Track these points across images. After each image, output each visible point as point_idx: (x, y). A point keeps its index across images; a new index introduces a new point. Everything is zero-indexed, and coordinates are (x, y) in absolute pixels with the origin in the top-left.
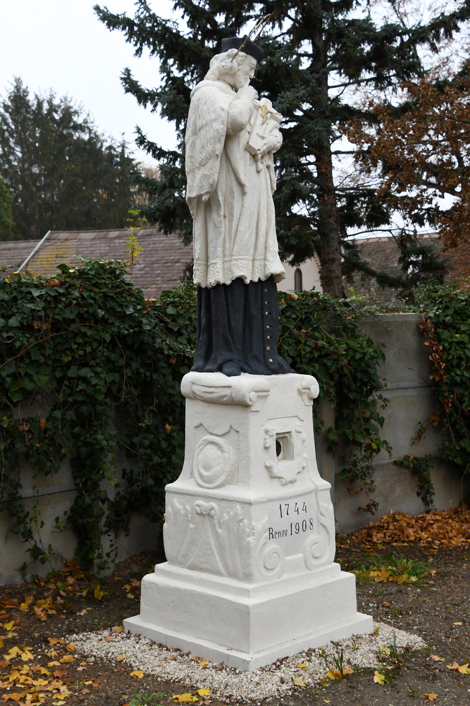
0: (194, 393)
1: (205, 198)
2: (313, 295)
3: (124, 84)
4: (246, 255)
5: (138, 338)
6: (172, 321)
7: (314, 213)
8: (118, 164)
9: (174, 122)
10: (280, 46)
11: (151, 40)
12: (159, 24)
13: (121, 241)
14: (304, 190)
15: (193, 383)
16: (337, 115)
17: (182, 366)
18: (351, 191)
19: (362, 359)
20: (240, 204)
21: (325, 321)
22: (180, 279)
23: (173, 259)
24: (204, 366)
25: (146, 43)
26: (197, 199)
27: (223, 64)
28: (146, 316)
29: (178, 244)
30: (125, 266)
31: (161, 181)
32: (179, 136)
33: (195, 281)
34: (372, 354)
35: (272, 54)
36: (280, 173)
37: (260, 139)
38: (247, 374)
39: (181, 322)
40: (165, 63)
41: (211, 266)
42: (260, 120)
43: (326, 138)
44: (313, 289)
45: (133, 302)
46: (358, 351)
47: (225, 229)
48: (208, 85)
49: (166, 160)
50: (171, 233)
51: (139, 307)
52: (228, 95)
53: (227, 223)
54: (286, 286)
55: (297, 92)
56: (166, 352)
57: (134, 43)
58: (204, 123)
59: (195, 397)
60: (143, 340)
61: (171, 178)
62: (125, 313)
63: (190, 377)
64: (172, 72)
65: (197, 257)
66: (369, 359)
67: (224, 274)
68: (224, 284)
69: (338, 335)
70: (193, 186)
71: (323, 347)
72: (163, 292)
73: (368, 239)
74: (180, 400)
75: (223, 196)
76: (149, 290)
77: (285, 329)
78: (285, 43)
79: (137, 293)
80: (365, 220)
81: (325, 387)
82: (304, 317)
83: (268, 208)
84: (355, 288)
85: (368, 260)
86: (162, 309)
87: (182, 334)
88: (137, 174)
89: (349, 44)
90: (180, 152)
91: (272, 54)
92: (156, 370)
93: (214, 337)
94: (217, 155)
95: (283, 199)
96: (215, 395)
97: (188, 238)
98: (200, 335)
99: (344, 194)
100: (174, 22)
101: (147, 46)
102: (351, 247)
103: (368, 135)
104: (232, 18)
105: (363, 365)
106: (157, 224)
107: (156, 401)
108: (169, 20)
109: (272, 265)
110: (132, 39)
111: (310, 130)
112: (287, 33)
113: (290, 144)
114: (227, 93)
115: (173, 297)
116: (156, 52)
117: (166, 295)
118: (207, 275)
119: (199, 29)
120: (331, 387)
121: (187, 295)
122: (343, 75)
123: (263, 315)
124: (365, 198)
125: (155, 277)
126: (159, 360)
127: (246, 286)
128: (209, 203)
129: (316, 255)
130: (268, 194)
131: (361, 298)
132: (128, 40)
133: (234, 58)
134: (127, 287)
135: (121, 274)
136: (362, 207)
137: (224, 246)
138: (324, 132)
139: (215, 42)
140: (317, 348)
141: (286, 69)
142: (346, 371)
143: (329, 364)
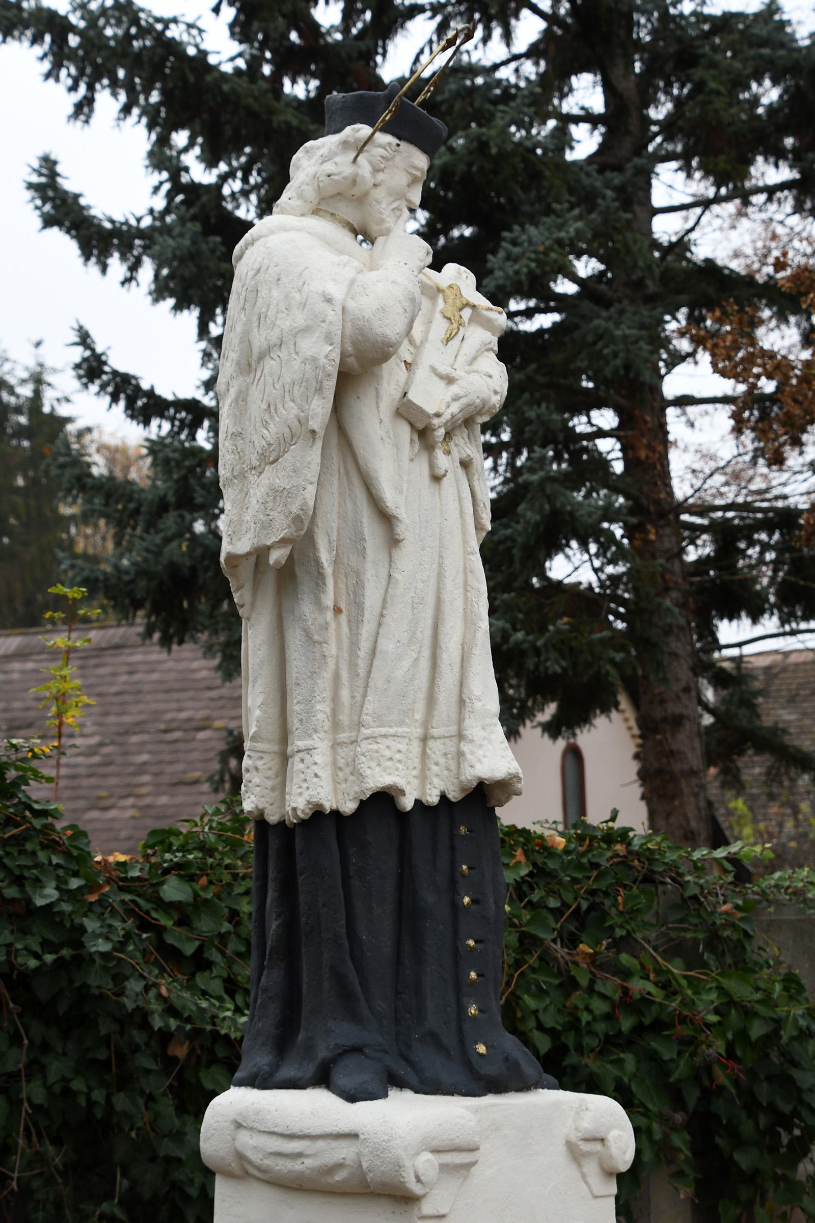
0: (240, 1157)
1: (277, 556)
2: (610, 837)
3: (39, 202)
4: (401, 723)
5: (71, 981)
6: (179, 923)
7: (614, 579)
8: (21, 432)
9: (191, 317)
10: (508, 93)
11: (121, 73)
12: (145, 31)
13: (30, 665)
14: (582, 512)
15: (239, 1126)
16: (679, 292)
17: (208, 1066)
18: (730, 514)
19: (772, 1038)
20: (384, 574)
21: (649, 917)
22: (210, 779)
23: (189, 720)
24: (275, 1067)
25: (106, 82)
26: (253, 559)
27: (329, 167)
28: (98, 909)
29: (204, 674)
30: (35, 756)
31: (154, 486)
32: (207, 355)
33: (248, 805)
34: (802, 1023)
35: (485, 119)
36: (511, 464)
37: (442, 384)
38: (408, 1094)
39: (205, 925)
40: (163, 141)
41: (297, 758)
42: (440, 327)
43: (647, 361)
44: (613, 819)
45: (58, 866)
46: (756, 1014)
47: (339, 648)
48: (283, 229)
49: (166, 427)
50: (181, 642)
51: (75, 883)
52: (345, 258)
53: (345, 629)
54: (534, 809)
55: (560, 228)
56: (157, 1023)
57: (70, 82)
58: (274, 339)
59: (245, 1171)
60: (85, 986)
61: (185, 478)
62: (29, 902)
63: (232, 1103)
64: (186, 169)
65: (253, 730)
66: (793, 1038)
67: (336, 782)
68: (336, 813)
69: (694, 962)
70: (241, 522)
71: (646, 1000)
72: (153, 833)
73: (787, 654)
74: (198, 1179)
75: (330, 550)
76: (113, 813)
77: (527, 942)
78: (522, 84)
79: (71, 838)
80: (772, 599)
81: (658, 1131)
82: (584, 905)
83: (466, 583)
84: (751, 800)
85: (787, 716)
86: (146, 888)
87: (208, 965)
88: (77, 466)
89: (713, 85)
90: (208, 401)
91: (485, 119)
92: (126, 1082)
93: (305, 978)
94: (313, 432)
95: (520, 540)
96: (309, 1162)
97: (231, 664)
98: (261, 968)
99: (705, 522)
100: (190, 26)
101: (107, 92)
102: (734, 678)
103: (771, 355)
104: (363, 11)
105: (775, 1057)
106: (141, 613)
107: (122, 1183)
108: (175, 20)
109: (480, 752)
110: (63, 73)
111: (600, 337)
112: (527, 55)
113: (540, 378)
114: (341, 252)
115: (183, 849)
116: (136, 111)
117: (162, 842)
118: (283, 784)
119: (263, 46)
120: (675, 1129)
121: (227, 841)
122: (698, 175)
123: (455, 906)
124: (770, 536)
125: (135, 774)
126: (135, 1049)
127: (402, 816)
128: (291, 571)
129: (624, 701)
130: (465, 542)
131: (758, 849)
132: (52, 74)
133: (360, 151)
134: (37, 823)
135: (23, 780)
136: (761, 561)
137: (335, 699)
138: (642, 344)
139: (314, 84)
140: (629, 1003)
141: (524, 160)
142: (721, 1077)
143: (667, 1053)
